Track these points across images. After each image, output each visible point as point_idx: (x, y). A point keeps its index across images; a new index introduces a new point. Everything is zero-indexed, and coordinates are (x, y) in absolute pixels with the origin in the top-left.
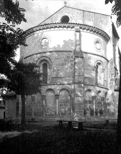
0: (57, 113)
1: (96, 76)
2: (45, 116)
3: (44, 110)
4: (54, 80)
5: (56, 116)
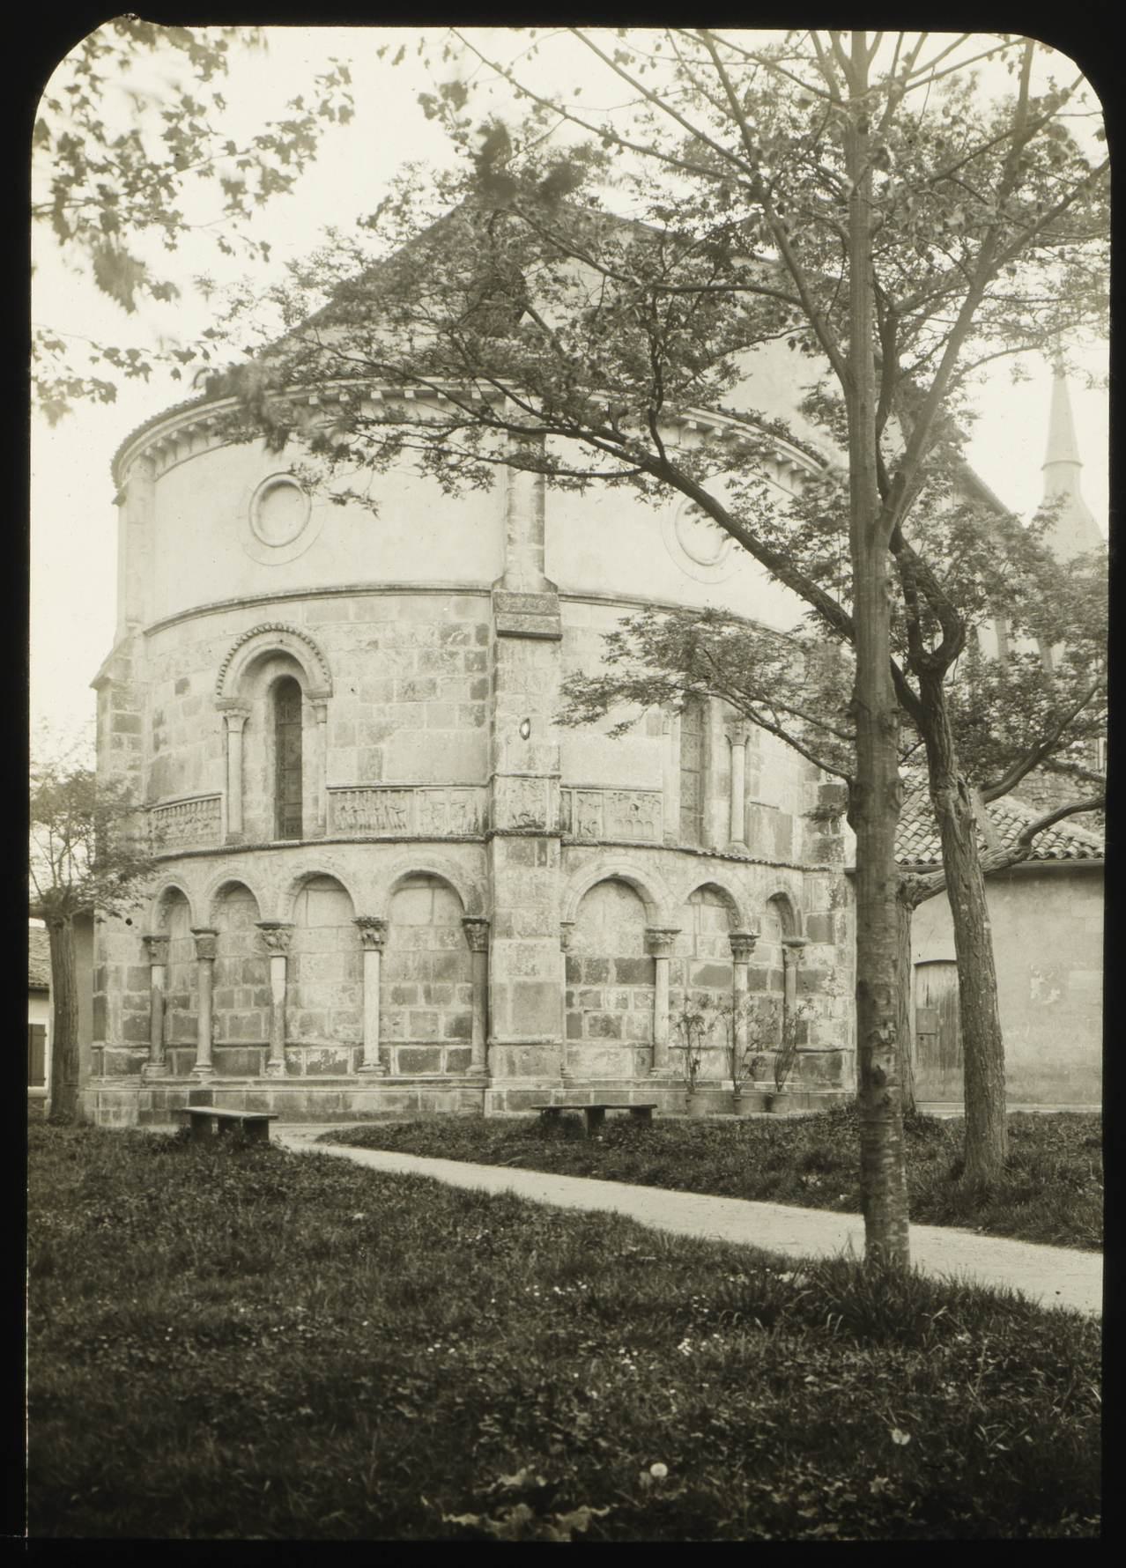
0: (371, 1055)
1: (997, 298)
2: (280, 1073)
3: (278, 1032)
4: (348, 806)
5: (361, 1078)
